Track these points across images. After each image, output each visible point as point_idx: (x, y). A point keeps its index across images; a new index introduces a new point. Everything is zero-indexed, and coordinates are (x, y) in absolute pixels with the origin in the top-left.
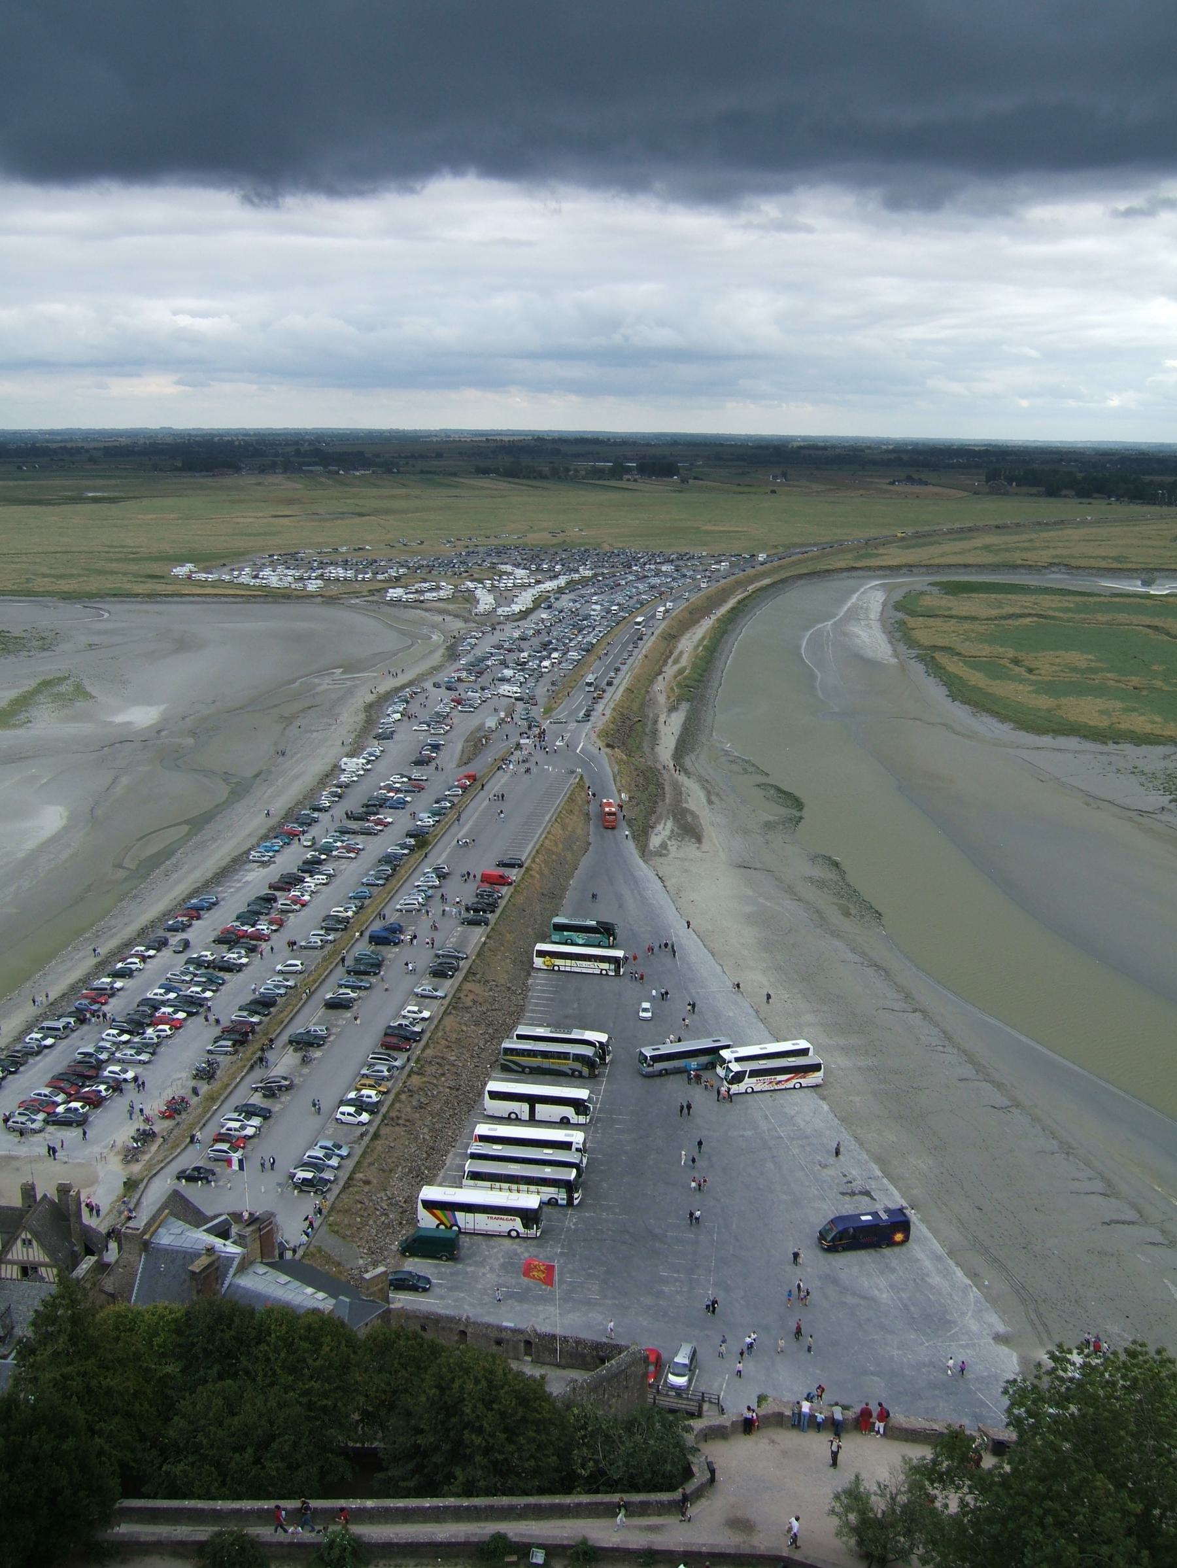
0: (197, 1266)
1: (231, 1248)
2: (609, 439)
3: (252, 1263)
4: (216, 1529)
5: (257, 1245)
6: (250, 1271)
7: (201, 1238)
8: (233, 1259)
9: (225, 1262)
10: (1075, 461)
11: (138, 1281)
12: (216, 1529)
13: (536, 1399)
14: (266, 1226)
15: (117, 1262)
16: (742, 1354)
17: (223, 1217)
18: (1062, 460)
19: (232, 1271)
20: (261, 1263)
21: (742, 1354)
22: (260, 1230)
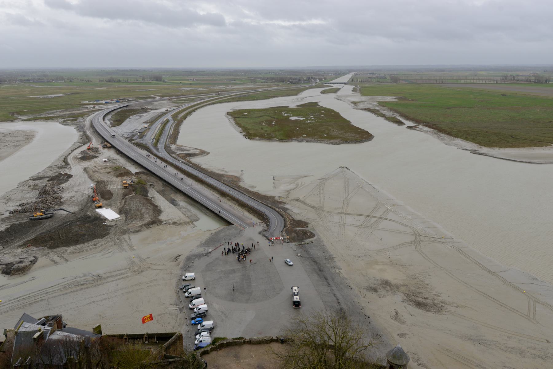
0: (36, 335)
1: (47, 328)
2: (140, 70)
3: (54, 331)
4: (144, 171)
5: (56, 325)
6: (54, 333)
7: (34, 327)
8: (48, 331)
9: (45, 333)
10: (274, 73)
11: (14, 345)
12: (144, 171)
13: (229, 199)
14: (58, 319)
15: (5, 341)
16: (272, 258)
17: (43, 319)
18: (270, 73)
19: (48, 335)
20: (58, 330)
21: (272, 258)
22: (56, 320)
